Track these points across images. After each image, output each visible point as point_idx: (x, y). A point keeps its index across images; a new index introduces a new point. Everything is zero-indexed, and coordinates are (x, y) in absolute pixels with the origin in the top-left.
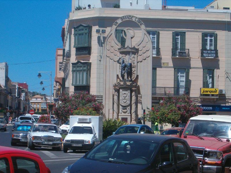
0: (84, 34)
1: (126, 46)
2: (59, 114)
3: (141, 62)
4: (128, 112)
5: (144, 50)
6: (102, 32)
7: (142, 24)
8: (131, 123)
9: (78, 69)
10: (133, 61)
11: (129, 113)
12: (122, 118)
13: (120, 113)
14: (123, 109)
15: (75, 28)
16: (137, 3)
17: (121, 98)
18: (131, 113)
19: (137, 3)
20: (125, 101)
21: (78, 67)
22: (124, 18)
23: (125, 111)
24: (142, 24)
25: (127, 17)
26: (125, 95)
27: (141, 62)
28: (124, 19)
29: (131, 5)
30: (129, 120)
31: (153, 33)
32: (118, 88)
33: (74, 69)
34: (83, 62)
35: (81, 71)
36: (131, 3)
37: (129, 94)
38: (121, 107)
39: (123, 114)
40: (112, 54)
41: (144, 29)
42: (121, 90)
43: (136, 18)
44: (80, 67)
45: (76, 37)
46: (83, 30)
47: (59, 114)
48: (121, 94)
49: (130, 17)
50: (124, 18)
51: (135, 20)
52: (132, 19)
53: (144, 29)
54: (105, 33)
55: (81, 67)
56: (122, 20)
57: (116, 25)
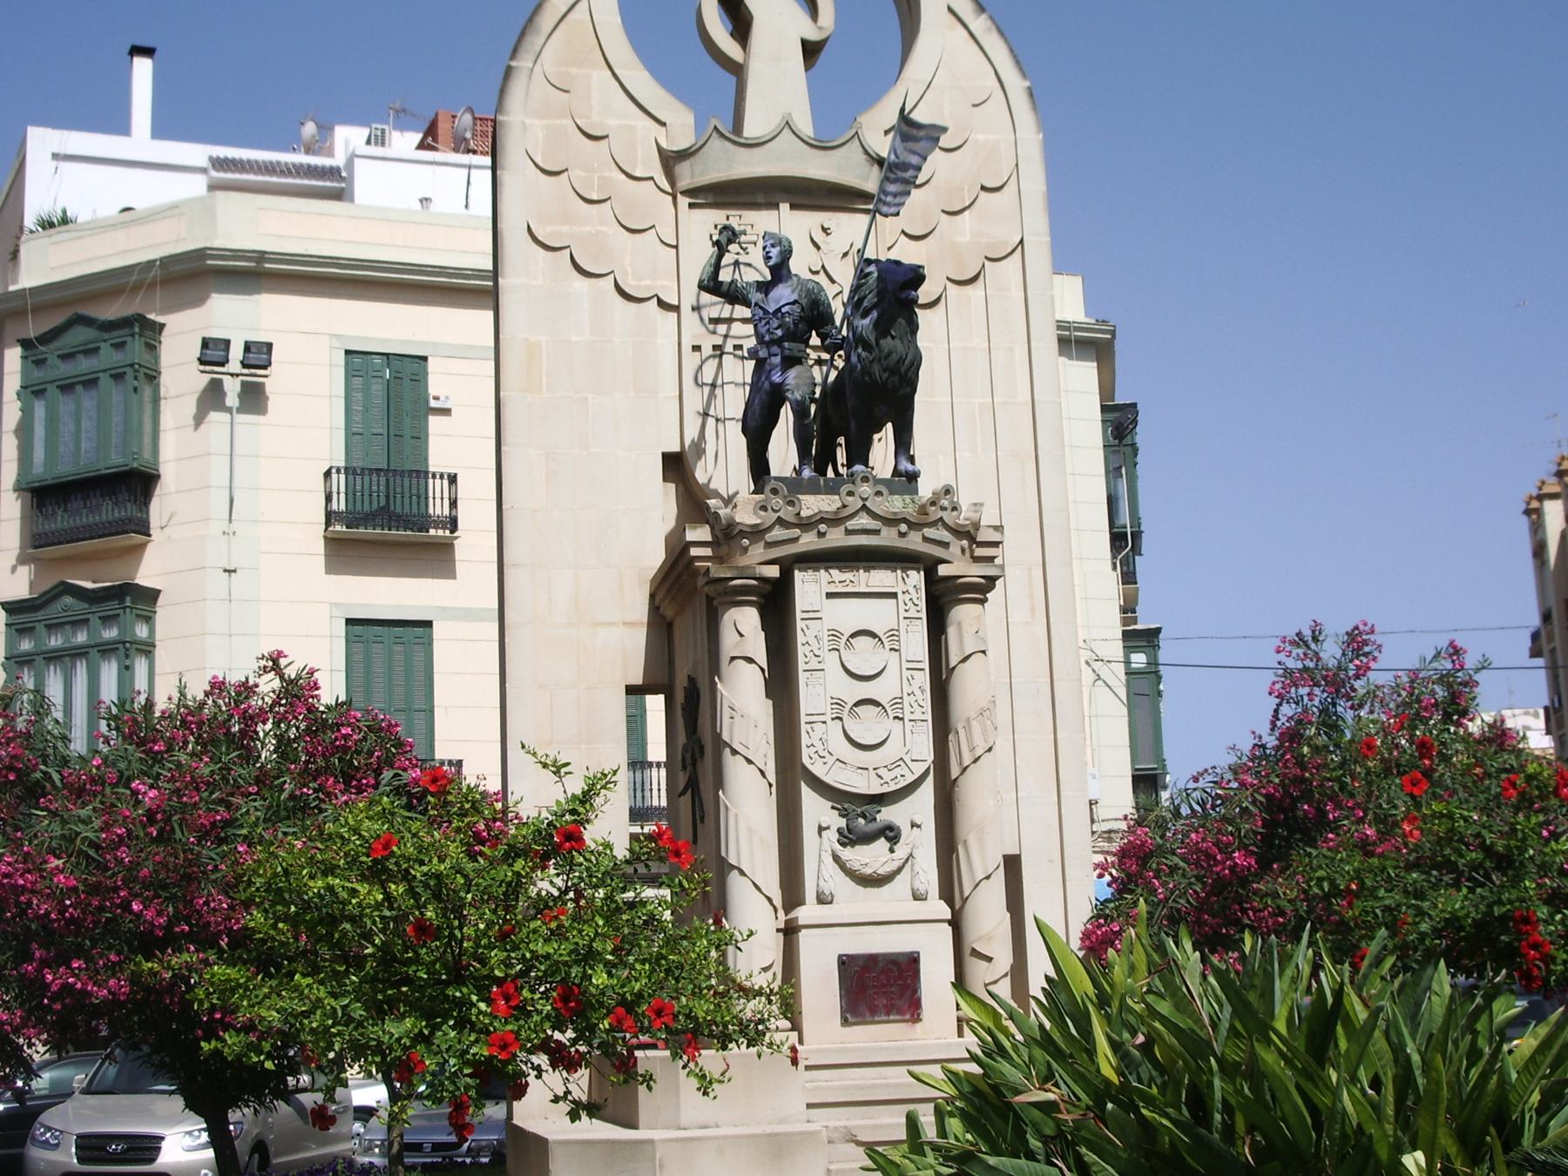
0: (105, 380)
1: (754, 127)
6: (245, 365)
9: (55, 642)
11: (934, 890)
12: (845, 962)
13: (810, 895)
14: (843, 845)
15: (26, 344)
17: (812, 696)
18: (948, 890)
20: (868, 727)
21: (52, 627)
23: (874, 856)
26: (864, 657)
32: (773, 572)
33: (26, 645)
34: (93, 591)
35: (79, 653)
37: (916, 642)
38: (815, 810)
39: (853, 902)
40: (599, 222)
42: (809, 588)
44: (67, 627)
45: (40, 409)
46: (92, 352)
48: (808, 638)
54: (265, 367)
55: (78, 623)
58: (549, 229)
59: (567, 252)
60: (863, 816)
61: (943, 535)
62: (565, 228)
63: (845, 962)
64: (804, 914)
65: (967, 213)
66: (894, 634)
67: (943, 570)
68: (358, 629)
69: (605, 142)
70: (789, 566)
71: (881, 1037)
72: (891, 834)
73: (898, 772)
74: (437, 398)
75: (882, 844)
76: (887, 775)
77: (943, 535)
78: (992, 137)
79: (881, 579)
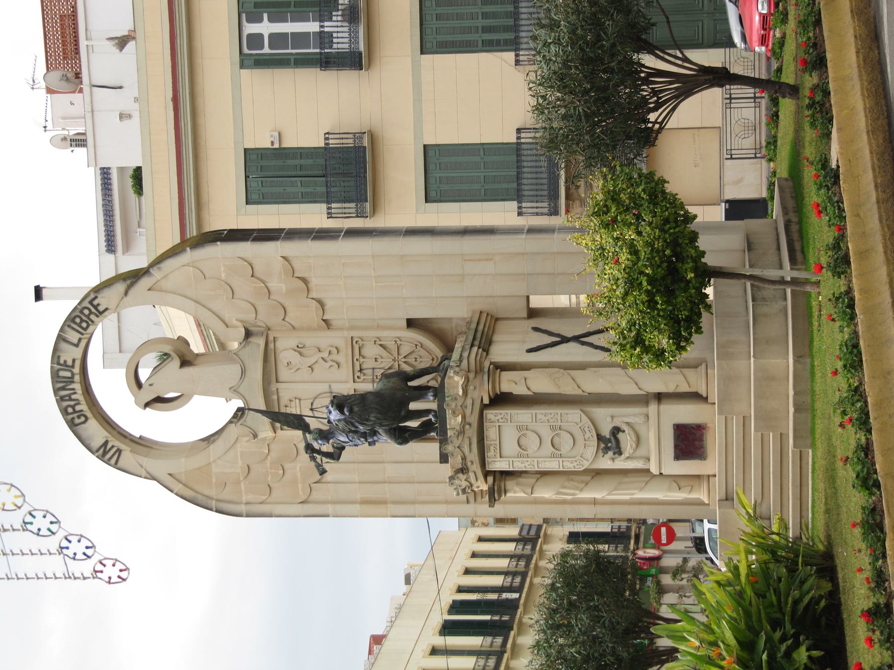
2: (683, 263)
3: (321, 303)
4: (637, 420)
5: (244, 287)
7: (96, 307)
8: (705, 399)
10: (325, 355)
16: (121, 87)
17: (552, 465)
19: (121, 87)
20: (566, 442)
22: (73, 407)
24: (96, 307)
25: (63, 388)
26: (532, 442)
27: (321, 303)
28: (78, 408)
29: (130, 116)
30: (687, 413)
31: (248, 21)
36: (122, 116)
37: (522, 415)
41: (126, 293)
43: (66, 341)
47: (683, 263)
49: (62, 374)
50: (73, 407)
51: (77, 345)
52: (73, 366)
53: (126, 293)
56: (85, 416)
57: (119, 451)
58: (301, 493)
59: (312, 485)
60: (610, 443)
61: (469, 402)
62: (300, 486)
63: (677, 458)
64: (654, 470)
65: (269, 285)
66: (519, 428)
67: (486, 401)
68: (424, 50)
69: (251, 467)
70: (486, 474)
71: (714, 442)
72: (616, 430)
73: (586, 429)
74: (272, 143)
75: (620, 436)
76: (588, 435)
77: (469, 402)
78: (222, 269)
79: (491, 433)
